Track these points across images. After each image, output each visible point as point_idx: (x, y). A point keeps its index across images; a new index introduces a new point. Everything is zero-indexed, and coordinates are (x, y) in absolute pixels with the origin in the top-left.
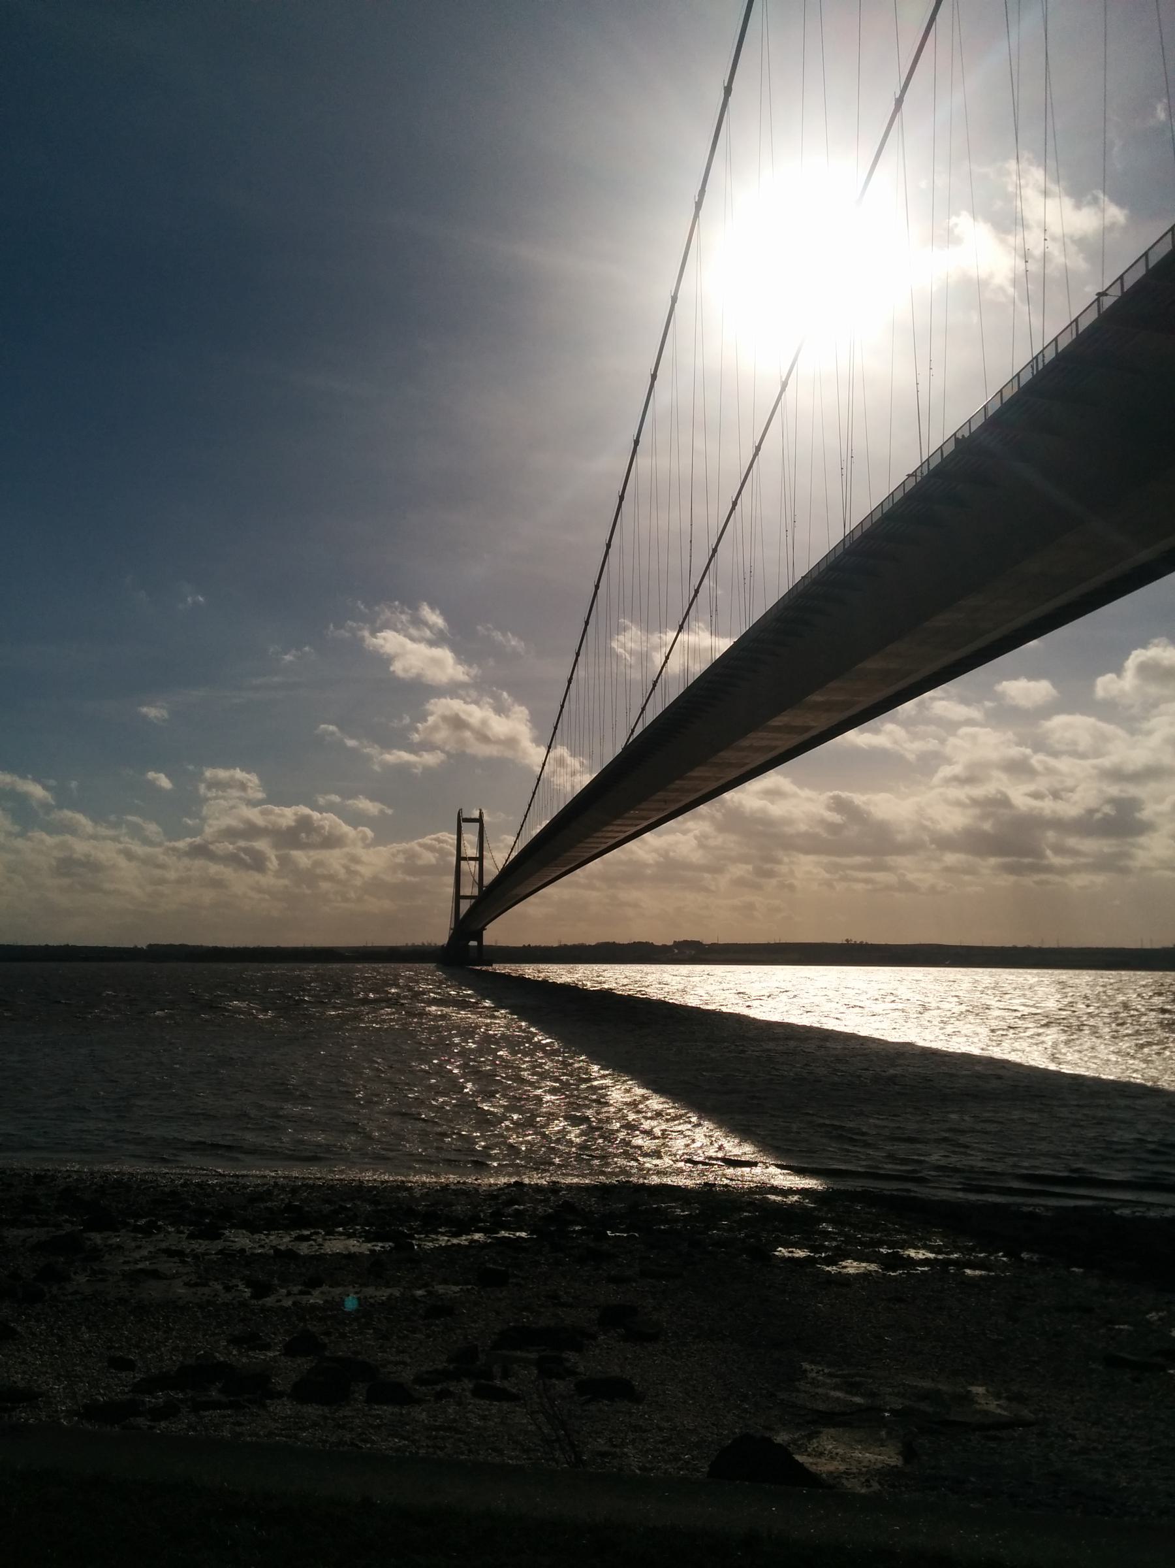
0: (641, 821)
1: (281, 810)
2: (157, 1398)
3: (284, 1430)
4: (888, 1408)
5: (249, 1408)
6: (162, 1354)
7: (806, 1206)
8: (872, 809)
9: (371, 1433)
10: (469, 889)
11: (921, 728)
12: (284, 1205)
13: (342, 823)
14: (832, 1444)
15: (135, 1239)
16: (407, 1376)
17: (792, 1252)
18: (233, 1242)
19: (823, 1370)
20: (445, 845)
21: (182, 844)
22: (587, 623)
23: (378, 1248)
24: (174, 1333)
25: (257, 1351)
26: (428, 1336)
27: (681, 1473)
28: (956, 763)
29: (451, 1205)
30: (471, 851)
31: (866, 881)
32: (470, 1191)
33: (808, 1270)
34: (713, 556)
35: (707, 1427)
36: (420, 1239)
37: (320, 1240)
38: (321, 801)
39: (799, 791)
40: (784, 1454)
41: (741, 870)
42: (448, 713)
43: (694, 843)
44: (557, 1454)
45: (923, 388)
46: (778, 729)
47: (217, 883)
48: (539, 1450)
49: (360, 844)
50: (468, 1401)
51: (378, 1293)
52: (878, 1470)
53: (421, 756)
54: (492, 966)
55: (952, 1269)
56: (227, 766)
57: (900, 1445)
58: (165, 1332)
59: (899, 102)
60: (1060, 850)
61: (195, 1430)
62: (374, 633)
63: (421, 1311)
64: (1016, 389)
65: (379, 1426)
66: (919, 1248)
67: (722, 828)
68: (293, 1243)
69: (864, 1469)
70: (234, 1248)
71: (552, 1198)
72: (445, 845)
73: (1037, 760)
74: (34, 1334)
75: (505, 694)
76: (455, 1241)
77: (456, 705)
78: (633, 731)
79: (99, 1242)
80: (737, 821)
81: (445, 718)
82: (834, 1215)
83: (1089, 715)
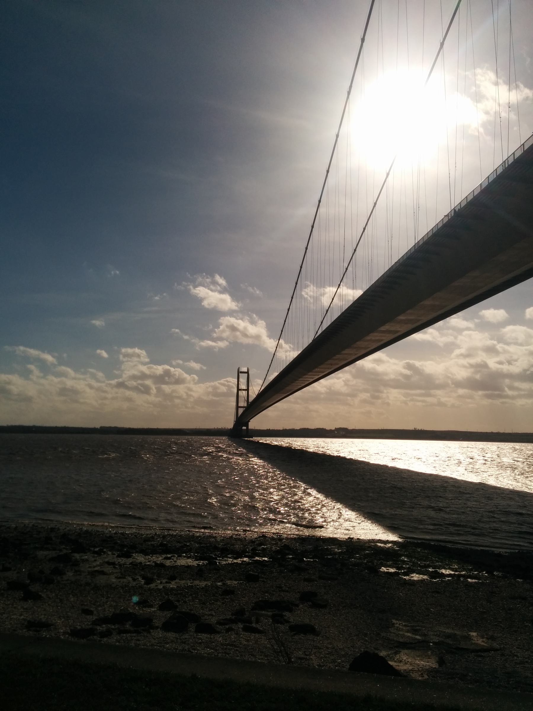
0: (320, 373)
1: (157, 367)
2: (103, 627)
3: (158, 643)
4: (432, 641)
5: (143, 633)
6: (105, 609)
7: (395, 549)
8: (425, 368)
9: (197, 646)
10: (242, 404)
11: (445, 331)
12: (159, 543)
13: (184, 373)
14: (406, 657)
15: (94, 557)
16: (214, 621)
17: (388, 569)
18: (137, 559)
19: (402, 623)
20: (230, 383)
21: (114, 382)
22: (296, 284)
23: (201, 564)
24: (110, 599)
25: (147, 608)
26: (223, 603)
27: (337, 668)
28: (462, 348)
29: (234, 545)
30: (243, 386)
31: (423, 401)
32: (242, 539)
33: (396, 578)
34: (354, 252)
35: (349, 648)
36: (220, 560)
37: (175, 559)
38: (174, 363)
39: (390, 360)
40: (383, 660)
41: (364, 396)
42: (229, 324)
43: (343, 383)
44: (281, 658)
45: (452, 173)
46: (383, 332)
47: (129, 400)
48: (272, 656)
49: (192, 383)
50: (240, 633)
51: (201, 584)
52: (427, 669)
53: (217, 343)
54: (252, 438)
55: (462, 579)
56: (132, 347)
57: (437, 658)
58: (107, 598)
59: (442, 44)
60: (511, 388)
61: (119, 642)
62: (195, 287)
63: (220, 592)
65: (200, 643)
66: (447, 569)
67: (355, 376)
68: (163, 560)
69: (420, 669)
70: (137, 562)
71: (279, 543)
72: (230, 383)
73: (500, 347)
74: (49, 598)
75: (255, 316)
76: (235, 561)
77: (232, 320)
78: (317, 332)
79: (78, 558)
80: (363, 374)
81: (227, 326)
82: (407, 553)
83: (524, 326)
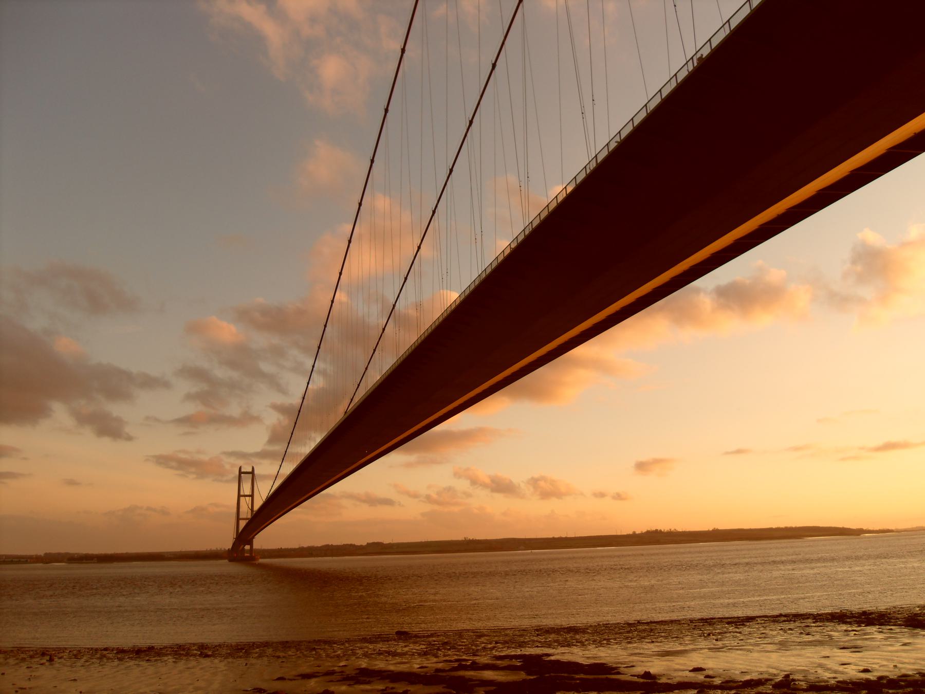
59: (283, 459)
64: (565, 195)
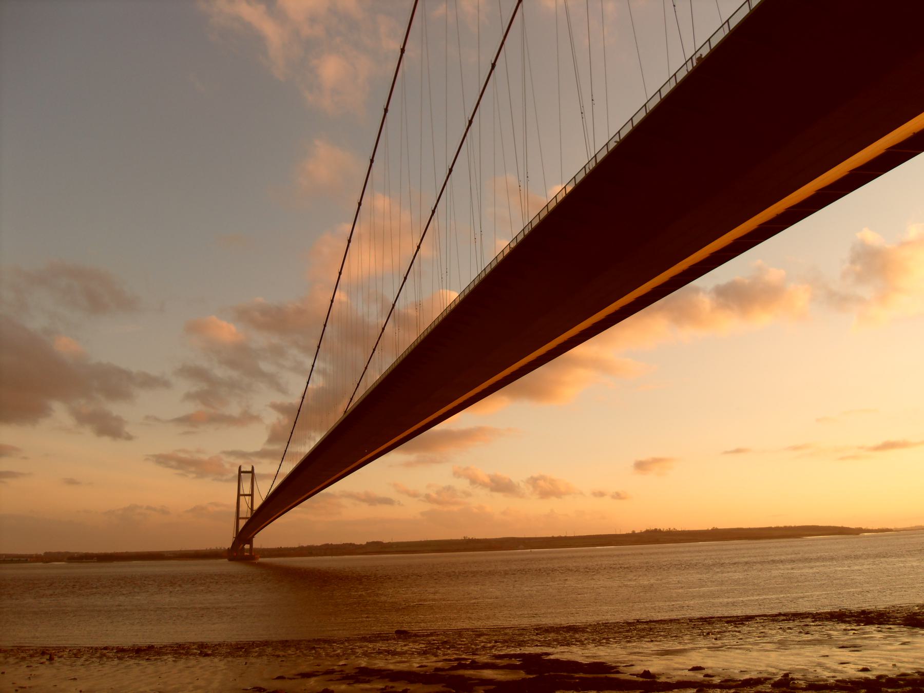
64: (564, 195)
